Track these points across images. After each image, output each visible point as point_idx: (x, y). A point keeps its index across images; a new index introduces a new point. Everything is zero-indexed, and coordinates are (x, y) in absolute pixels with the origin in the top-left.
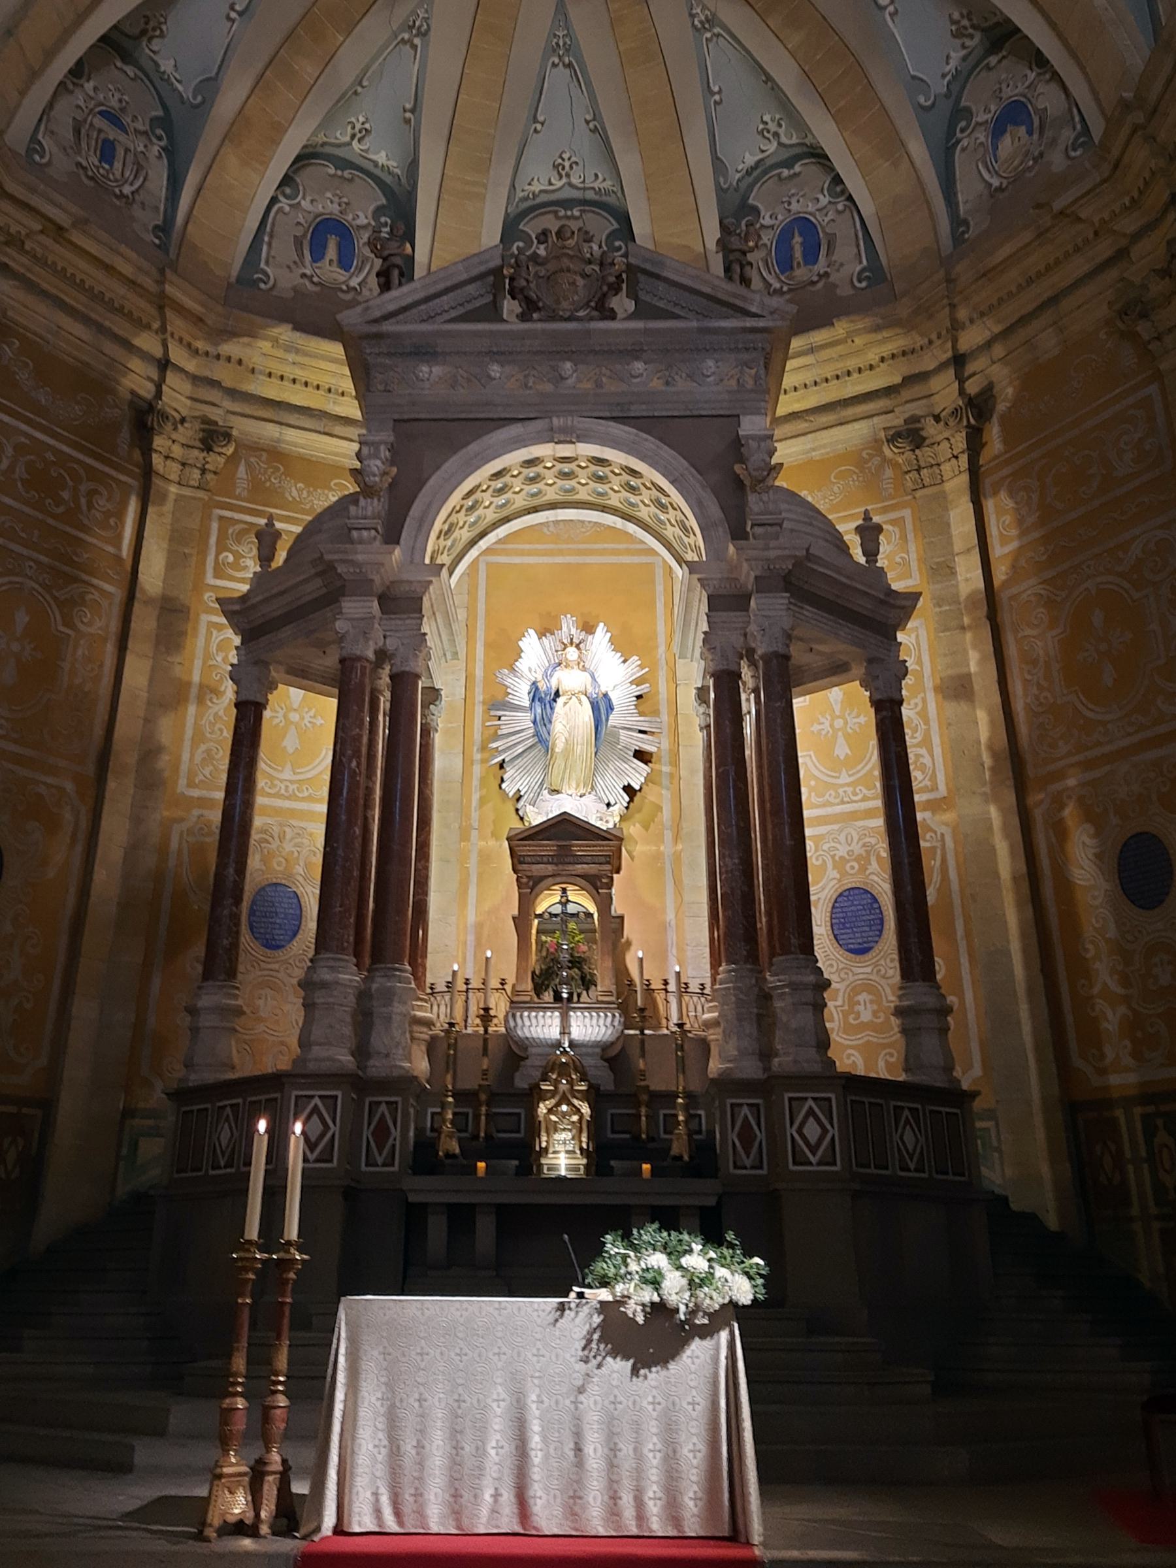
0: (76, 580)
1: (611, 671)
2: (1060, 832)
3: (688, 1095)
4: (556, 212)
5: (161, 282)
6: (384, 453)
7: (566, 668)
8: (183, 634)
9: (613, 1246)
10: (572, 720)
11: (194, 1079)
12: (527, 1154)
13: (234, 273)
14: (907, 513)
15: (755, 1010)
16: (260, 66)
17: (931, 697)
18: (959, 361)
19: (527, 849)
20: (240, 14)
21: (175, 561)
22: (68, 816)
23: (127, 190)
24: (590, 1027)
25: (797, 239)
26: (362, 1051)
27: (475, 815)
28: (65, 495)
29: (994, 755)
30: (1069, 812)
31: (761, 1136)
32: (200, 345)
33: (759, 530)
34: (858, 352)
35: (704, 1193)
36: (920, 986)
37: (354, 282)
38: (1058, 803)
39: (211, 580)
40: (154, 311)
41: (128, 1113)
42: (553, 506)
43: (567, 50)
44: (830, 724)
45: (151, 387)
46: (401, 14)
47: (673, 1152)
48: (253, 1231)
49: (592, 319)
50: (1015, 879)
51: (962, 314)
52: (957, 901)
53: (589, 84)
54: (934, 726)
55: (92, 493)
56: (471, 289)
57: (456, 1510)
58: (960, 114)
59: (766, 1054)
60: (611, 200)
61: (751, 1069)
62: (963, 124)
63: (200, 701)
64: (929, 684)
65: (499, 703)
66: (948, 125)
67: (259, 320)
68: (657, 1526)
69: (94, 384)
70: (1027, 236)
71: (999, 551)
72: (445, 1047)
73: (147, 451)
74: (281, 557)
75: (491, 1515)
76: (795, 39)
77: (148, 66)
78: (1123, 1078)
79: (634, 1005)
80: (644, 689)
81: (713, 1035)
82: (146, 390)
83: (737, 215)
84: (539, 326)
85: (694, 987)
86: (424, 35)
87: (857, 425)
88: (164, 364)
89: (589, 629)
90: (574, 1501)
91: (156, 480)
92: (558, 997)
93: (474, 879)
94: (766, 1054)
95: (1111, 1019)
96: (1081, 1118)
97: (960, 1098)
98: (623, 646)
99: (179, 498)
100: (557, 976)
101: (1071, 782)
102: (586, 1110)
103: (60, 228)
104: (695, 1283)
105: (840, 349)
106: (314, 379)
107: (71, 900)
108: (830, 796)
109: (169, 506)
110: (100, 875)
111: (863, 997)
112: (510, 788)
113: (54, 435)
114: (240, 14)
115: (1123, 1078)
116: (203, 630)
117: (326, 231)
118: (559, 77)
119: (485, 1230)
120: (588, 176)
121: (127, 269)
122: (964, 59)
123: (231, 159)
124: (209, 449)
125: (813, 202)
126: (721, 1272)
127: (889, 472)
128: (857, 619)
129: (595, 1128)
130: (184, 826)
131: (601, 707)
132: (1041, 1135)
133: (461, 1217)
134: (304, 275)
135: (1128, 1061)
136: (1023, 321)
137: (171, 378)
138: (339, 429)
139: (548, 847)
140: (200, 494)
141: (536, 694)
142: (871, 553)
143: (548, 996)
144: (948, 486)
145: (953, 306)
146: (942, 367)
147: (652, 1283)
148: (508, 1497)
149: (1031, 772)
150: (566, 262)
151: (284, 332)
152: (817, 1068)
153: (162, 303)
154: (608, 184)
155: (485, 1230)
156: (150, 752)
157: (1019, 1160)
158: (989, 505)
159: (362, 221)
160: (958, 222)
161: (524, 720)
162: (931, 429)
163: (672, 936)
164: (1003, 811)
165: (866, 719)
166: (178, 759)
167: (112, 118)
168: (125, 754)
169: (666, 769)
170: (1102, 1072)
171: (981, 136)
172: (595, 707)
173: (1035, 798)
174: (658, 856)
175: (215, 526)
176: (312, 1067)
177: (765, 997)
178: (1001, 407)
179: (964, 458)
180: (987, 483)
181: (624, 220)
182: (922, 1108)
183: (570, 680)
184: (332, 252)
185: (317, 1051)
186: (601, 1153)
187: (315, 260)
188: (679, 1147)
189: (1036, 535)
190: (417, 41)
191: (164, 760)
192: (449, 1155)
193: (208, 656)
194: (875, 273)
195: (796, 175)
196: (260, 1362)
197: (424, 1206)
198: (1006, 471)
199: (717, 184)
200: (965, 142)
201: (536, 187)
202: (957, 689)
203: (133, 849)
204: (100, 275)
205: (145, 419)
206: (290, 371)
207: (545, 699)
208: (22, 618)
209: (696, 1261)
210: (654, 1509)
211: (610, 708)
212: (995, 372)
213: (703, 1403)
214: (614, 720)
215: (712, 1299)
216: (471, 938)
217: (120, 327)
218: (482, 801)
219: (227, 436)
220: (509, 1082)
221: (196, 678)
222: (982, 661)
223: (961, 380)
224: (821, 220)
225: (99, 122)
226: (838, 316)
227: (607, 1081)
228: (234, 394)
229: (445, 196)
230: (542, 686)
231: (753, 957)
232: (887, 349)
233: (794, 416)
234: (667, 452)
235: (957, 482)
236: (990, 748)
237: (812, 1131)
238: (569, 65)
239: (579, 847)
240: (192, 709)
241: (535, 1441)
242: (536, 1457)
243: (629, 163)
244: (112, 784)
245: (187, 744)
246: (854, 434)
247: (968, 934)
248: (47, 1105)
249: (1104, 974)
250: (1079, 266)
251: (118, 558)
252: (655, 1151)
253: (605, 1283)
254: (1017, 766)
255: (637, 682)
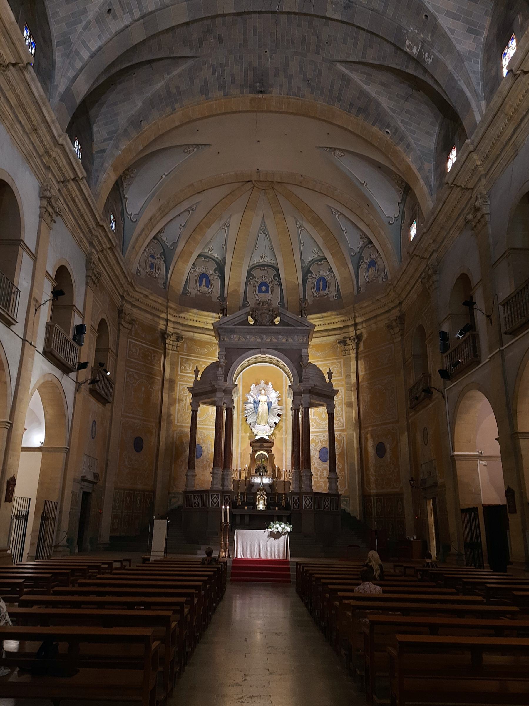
0: (152, 378)
1: (273, 396)
2: (367, 440)
3: (285, 494)
4: (260, 268)
5: (168, 302)
6: (224, 358)
7: (263, 400)
8: (174, 387)
9: (272, 524)
10: (263, 408)
11: (188, 489)
12: (255, 505)
13: (181, 292)
14: (342, 360)
15: (299, 478)
16: (187, 238)
17: (344, 406)
18: (356, 325)
19: (254, 444)
20: (183, 227)
21: (172, 369)
22: (154, 431)
23: (157, 275)
24: (266, 481)
25: (321, 283)
26: (223, 485)
27: (240, 428)
28: (149, 358)
29: (355, 421)
30: (369, 435)
31: (299, 503)
32: (175, 315)
33: (304, 379)
34: (333, 319)
35: (288, 513)
36: (332, 474)
37: (210, 291)
38: (367, 433)
39: (179, 373)
40: (165, 309)
41: (169, 493)
42: (260, 362)
43: (265, 230)
44: (318, 416)
45: (165, 327)
46: (222, 222)
47: (282, 506)
48: (223, 521)
49: (270, 326)
50: (357, 449)
51: (357, 315)
52: (345, 452)
53: (270, 238)
54: (344, 412)
55: (154, 356)
56: (243, 316)
57: (251, 555)
58: (361, 258)
59: (300, 488)
60: (275, 265)
61: (297, 490)
62: (362, 261)
63: (179, 403)
64: (344, 402)
65: (246, 402)
66: (358, 260)
67: (189, 308)
68: (277, 558)
69: (152, 329)
70: (371, 302)
71: (361, 374)
72: (237, 483)
73: (165, 344)
74: (199, 376)
75: (256, 556)
76: (323, 234)
77: (160, 239)
78: (373, 491)
79: (275, 473)
80: (280, 399)
81: (291, 481)
82: (164, 328)
83: (306, 273)
84: (258, 327)
85: (288, 471)
86: (228, 227)
87: (332, 337)
88: (167, 320)
89: (267, 384)
90: (266, 555)
91: (167, 350)
92: (260, 474)
93: (240, 442)
94: (300, 488)
95: (372, 479)
96: (365, 498)
97: (338, 495)
98: (275, 388)
99: (172, 354)
100: (260, 471)
101: (370, 429)
102: (266, 497)
103: (147, 296)
104: (283, 529)
105: (330, 318)
106: (201, 320)
107: (156, 449)
108: (320, 426)
109: (170, 356)
110: (161, 444)
111: (325, 471)
112: (248, 422)
113: (146, 344)
114: (183, 227)
115: (373, 491)
116: (178, 386)
117: (203, 277)
118: (262, 236)
119: (247, 519)
120: (269, 259)
121: (160, 301)
122: (363, 244)
123: (180, 263)
124: (178, 341)
125: (324, 273)
126: (286, 527)
127: (339, 350)
128: (324, 395)
129: (267, 500)
130: (177, 432)
131: (270, 404)
132: (358, 501)
133: (242, 517)
134: (197, 290)
135: (374, 488)
136: (370, 319)
137: (169, 324)
138: (207, 332)
139: (258, 444)
140: (177, 352)
141: (255, 401)
142: (330, 379)
143: (258, 474)
144: (351, 355)
145: (354, 313)
146: (352, 325)
147: (248, 475)
148: (258, 554)
149: (362, 426)
150: (264, 311)
151: (195, 310)
152: (310, 491)
153: (167, 307)
154: (274, 262)
155: (247, 519)
156: (169, 415)
157: (352, 506)
158: (359, 362)
159: (211, 273)
160: (359, 288)
161: (252, 406)
162: (348, 341)
163: (284, 456)
164: (356, 433)
165: (325, 416)
166: (175, 417)
167: (152, 256)
168: (164, 417)
169: (284, 418)
170: (370, 490)
171: (365, 266)
172: (268, 404)
173: (362, 431)
174: (282, 438)
175: (180, 360)
176: (214, 489)
177: (301, 477)
178: (364, 339)
179: (355, 350)
180: (359, 356)
181: (278, 270)
182: (333, 497)
183: (263, 398)
184: (204, 283)
185: (215, 486)
186: (268, 505)
187: (200, 286)
188: (283, 504)
189: (368, 372)
190: (226, 228)
191: (172, 417)
192: (239, 505)
193: (180, 392)
194: (339, 296)
195: (322, 264)
196: (225, 538)
197: (235, 515)
198: (363, 355)
199: (302, 266)
200: (362, 266)
201: (255, 262)
202: (349, 405)
203: (167, 438)
204: (154, 303)
205: (164, 335)
206: (195, 319)
207: (257, 403)
208: (143, 389)
209: (283, 526)
210: (276, 556)
211: (272, 404)
212: (362, 329)
213: (283, 544)
214: (272, 406)
215: (285, 531)
216: (239, 456)
217: (157, 313)
218: (242, 424)
219: (182, 338)
220: (250, 491)
221: (178, 397)
222: (355, 399)
223: (356, 330)
224: (328, 278)
225: (150, 259)
226: (329, 310)
227: (269, 491)
228: (183, 325)
229: (232, 267)
230: (256, 400)
231: (299, 469)
232: (340, 319)
233: (318, 331)
234: (286, 358)
235: (353, 356)
236: (355, 419)
237: (308, 502)
238: (265, 233)
239: (265, 444)
240: (177, 405)
241: (261, 548)
242: (261, 550)
243: (280, 259)
244: (162, 424)
245: (176, 413)
246: (332, 339)
247: (347, 459)
248: (154, 492)
249: (372, 470)
250: (381, 311)
251: (160, 371)
252: (278, 504)
253: (271, 528)
254: (360, 424)
255: (278, 397)
